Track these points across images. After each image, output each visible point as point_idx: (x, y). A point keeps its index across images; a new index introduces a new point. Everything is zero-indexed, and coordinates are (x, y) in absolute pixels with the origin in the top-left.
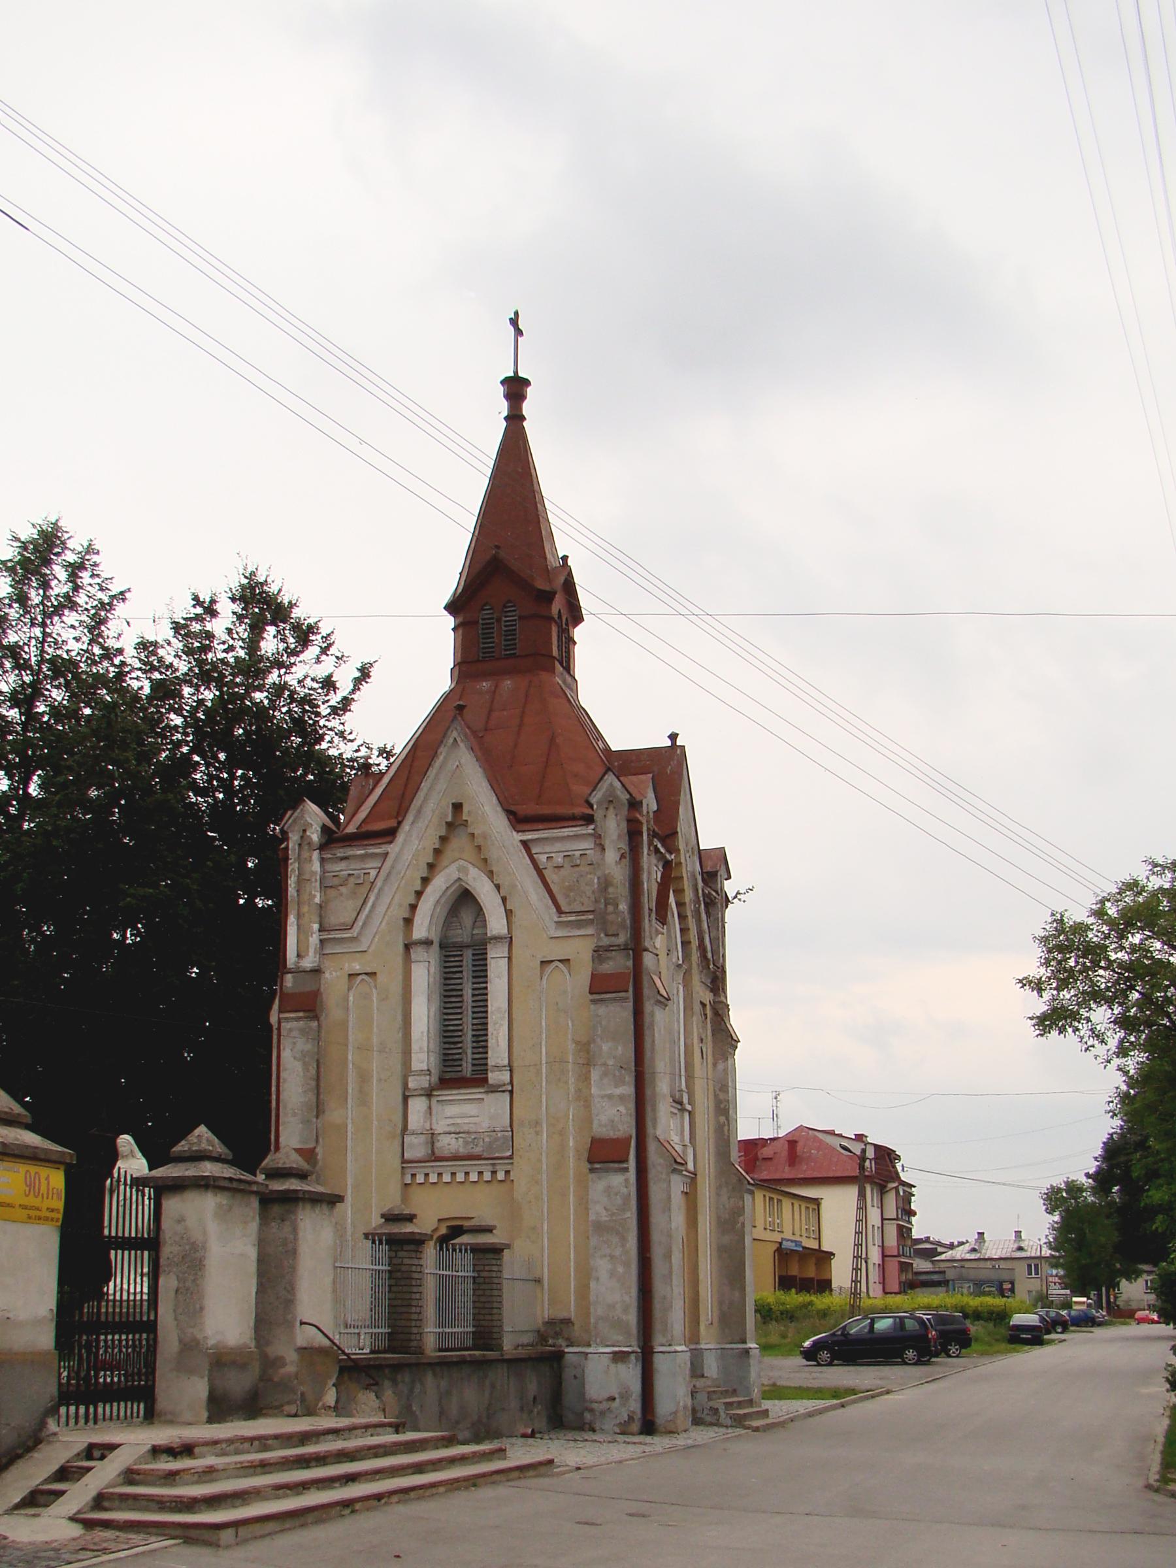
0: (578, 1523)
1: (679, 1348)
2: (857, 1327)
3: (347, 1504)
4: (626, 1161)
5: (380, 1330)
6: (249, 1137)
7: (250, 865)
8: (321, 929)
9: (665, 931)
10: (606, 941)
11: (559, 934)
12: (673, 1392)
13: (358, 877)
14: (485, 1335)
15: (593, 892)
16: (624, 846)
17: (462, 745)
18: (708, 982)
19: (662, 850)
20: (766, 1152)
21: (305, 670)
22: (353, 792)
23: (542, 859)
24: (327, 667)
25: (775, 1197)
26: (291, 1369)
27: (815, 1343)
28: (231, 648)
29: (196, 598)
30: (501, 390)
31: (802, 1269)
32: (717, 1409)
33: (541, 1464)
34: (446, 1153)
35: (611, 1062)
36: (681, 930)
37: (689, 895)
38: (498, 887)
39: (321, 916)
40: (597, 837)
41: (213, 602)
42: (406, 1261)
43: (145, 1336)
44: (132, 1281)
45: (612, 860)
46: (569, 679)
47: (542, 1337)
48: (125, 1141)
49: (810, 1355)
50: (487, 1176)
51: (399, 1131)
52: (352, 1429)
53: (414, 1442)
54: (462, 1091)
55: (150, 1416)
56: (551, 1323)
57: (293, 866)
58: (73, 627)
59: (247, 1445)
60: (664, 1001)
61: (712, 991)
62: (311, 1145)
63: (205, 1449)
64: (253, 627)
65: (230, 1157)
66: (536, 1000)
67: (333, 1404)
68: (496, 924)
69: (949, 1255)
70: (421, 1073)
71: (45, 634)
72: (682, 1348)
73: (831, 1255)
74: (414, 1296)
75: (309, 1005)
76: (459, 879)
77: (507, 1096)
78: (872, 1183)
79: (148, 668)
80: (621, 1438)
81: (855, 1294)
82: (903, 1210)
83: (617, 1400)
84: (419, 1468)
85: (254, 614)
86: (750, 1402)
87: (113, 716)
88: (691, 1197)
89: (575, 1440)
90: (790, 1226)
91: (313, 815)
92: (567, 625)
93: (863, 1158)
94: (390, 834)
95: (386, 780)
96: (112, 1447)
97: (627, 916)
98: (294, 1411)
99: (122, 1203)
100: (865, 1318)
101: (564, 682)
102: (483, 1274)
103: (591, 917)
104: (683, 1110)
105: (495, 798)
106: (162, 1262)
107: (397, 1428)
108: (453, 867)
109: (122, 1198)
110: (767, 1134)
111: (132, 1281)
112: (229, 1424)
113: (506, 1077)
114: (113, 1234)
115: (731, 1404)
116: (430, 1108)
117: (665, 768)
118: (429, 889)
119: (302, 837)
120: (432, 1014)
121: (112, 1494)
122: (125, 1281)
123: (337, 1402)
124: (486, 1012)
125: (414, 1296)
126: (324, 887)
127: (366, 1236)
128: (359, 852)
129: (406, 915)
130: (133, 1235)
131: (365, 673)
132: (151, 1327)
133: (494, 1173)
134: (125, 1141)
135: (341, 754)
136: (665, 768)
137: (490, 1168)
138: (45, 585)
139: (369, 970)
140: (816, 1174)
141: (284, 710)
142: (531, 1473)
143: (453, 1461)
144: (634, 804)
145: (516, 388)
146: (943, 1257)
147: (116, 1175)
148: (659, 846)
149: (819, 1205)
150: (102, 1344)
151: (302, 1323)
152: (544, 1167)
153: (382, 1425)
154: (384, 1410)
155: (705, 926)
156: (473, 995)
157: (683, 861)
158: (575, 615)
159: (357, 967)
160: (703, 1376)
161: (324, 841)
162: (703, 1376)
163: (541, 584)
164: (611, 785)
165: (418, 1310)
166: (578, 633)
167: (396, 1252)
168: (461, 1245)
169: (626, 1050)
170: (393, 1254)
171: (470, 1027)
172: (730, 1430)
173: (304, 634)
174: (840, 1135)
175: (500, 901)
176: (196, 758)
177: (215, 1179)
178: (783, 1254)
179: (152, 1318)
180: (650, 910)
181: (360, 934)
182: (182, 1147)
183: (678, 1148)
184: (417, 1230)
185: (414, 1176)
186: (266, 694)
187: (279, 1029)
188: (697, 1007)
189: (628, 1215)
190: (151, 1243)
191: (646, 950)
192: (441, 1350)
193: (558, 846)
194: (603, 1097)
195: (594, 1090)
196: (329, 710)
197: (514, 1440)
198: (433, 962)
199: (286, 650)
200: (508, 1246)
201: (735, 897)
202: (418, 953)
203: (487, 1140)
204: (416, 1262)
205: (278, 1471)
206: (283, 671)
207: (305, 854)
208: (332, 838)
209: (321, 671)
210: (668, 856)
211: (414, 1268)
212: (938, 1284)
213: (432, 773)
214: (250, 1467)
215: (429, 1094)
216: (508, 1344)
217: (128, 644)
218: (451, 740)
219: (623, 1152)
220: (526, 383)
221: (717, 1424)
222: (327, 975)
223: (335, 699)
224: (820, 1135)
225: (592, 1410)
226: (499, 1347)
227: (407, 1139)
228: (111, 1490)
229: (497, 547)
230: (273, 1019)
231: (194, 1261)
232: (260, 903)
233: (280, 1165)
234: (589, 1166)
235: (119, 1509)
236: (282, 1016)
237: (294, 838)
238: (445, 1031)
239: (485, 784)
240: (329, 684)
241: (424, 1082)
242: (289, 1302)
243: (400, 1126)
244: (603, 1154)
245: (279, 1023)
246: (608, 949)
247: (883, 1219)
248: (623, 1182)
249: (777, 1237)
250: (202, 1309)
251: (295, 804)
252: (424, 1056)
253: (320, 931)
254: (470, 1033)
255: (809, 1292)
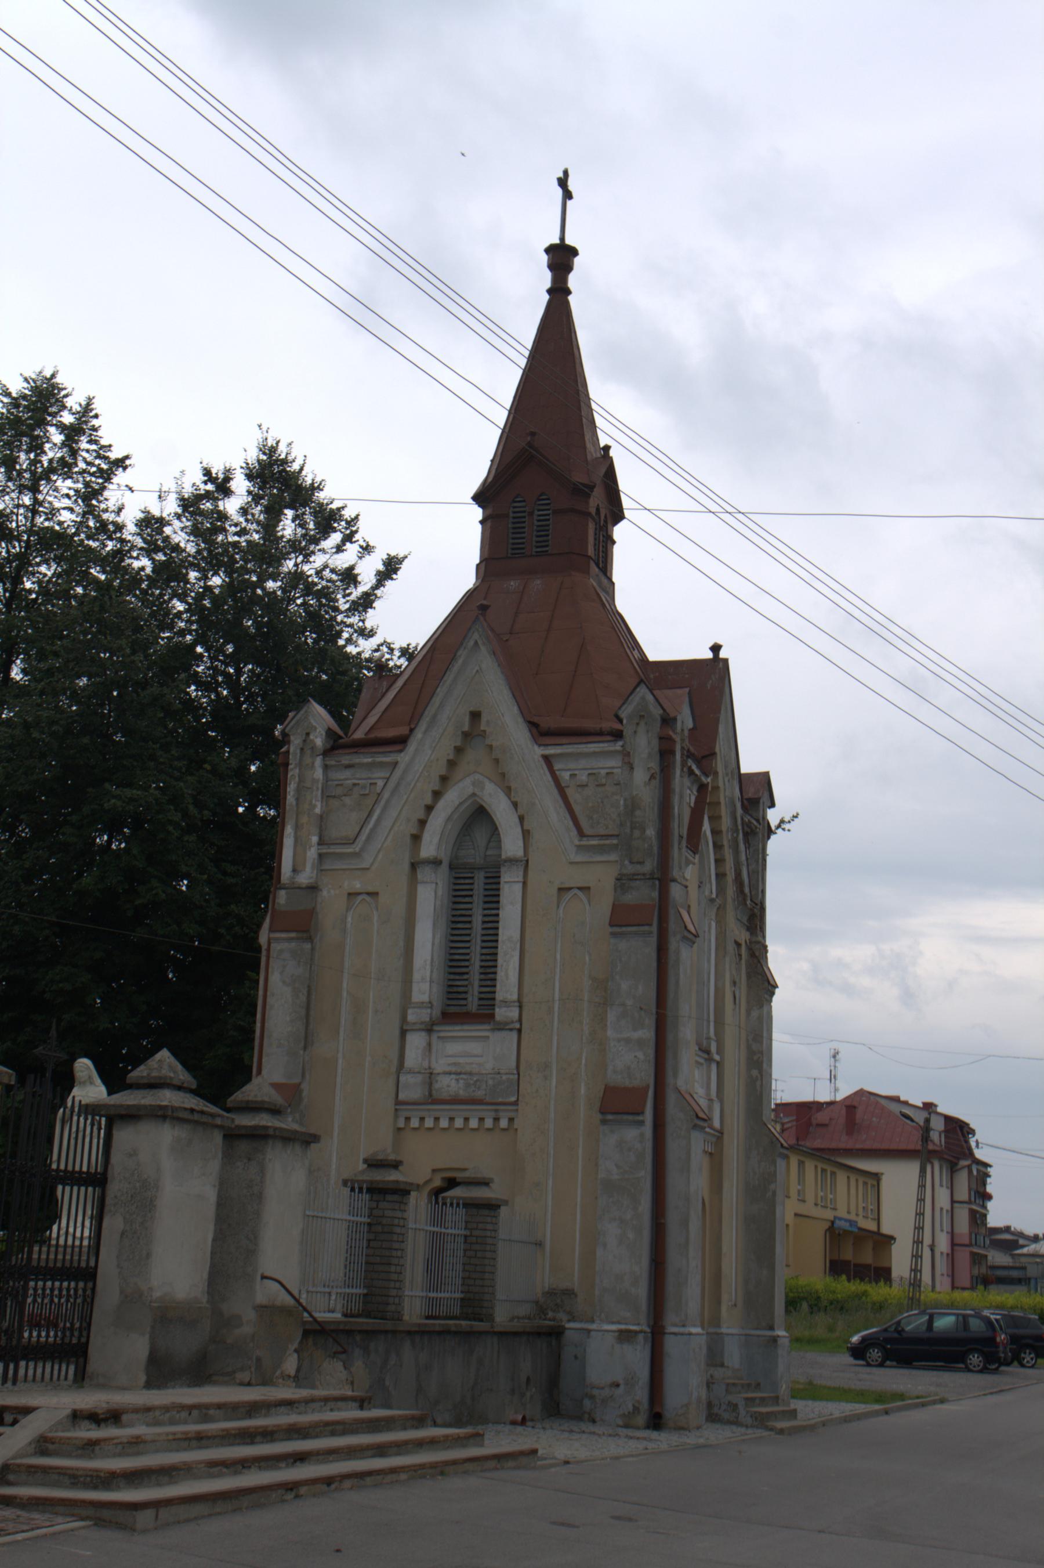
0: (554, 1523)
1: (694, 1330)
2: (914, 1323)
3: (291, 1487)
4: (642, 1113)
5: (354, 1291)
6: (222, 1065)
7: (253, 768)
8: (321, 843)
9: (696, 861)
10: (630, 869)
11: (579, 858)
12: (686, 1383)
13: (364, 787)
14: (475, 1304)
15: (619, 815)
16: (655, 765)
17: (483, 648)
18: (745, 919)
19: (697, 772)
20: (821, 1117)
21: (327, 557)
22: (365, 695)
23: (565, 776)
24: (348, 557)
25: (829, 1169)
26: (247, 1330)
27: (864, 1339)
28: (243, 532)
29: (207, 472)
30: (544, 258)
31: (858, 1253)
32: (736, 1405)
33: (522, 1453)
34: (444, 1095)
35: (629, 1002)
36: (716, 861)
37: (726, 823)
38: (515, 805)
39: (321, 828)
40: (626, 755)
41: (227, 479)
42: (388, 1213)
43: (81, 1284)
44: (79, 1224)
45: (641, 780)
46: (605, 581)
47: (541, 1310)
48: (84, 1066)
49: (858, 1352)
50: (489, 1123)
51: (394, 1069)
52: (309, 1401)
53: (378, 1420)
54: (466, 1027)
55: (81, 1378)
56: (551, 1293)
57: (293, 772)
58: (68, 496)
59: (184, 1414)
60: (691, 938)
61: (748, 929)
62: (296, 1081)
63: (135, 1416)
64: (267, 510)
65: (194, 1086)
66: (552, 928)
67: (293, 1373)
68: (512, 845)
69: (1032, 1248)
70: (421, 1005)
71: (36, 502)
72: (698, 1330)
73: (891, 1239)
74: (394, 1253)
75: (303, 925)
76: (474, 794)
77: (514, 1035)
78: (941, 1159)
79: (151, 549)
80: (620, 1431)
81: (916, 1283)
82: (977, 1192)
83: (622, 1387)
84: (381, 1450)
85: (272, 495)
86: (776, 1400)
87: (106, 598)
88: (716, 1158)
89: (571, 1431)
90: (845, 1202)
91: (318, 717)
92: (606, 521)
93: (927, 1129)
94: (401, 741)
95: (400, 682)
96: (27, 1411)
97: (655, 843)
98: (247, 1380)
99: (73, 1135)
100: (923, 1312)
101: (600, 583)
102: (475, 1233)
103: (615, 842)
104: (710, 1060)
105: (516, 708)
106: (109, 1200)
107: (362, 1403)
108: (468, 781)
109: (74, 1129)
110: (824, 1097)
111: (79, 1224)
112: (170, 1391)
113: (514, 1013)
114: (62, 1167)
115: (752, 1399)
116: (429, 1044)
117: (706, 681)
118: (441, 804)
119: (304, 741)
120: (437, 941)
121: (19, 1465)
122: (72, 1224)
123: (298, 1370)
124: (497, 941)
125: (394, 1253)
126: (327, 797)
127: (345, 1183)
128: (366, 760)
129: (414, 832)
130: (85, 1169)
131: (391, 567)
132: (90, 1275)
133: (496, 1120)
134: (84, 1066)
135: (359, 654)
136: (706, 681)
137: (493, 1114)
138: (37, 447)
139: (371, 889)
140: (885, 1146)
141: (299, 602)
142: (511, 1464)
143: (420, 1444)
144: (668, 721)
145: (561, 258)
146: (1025, 1250)
147: (69, 1104)
148: (694, 767)
149: (879, 1181)
150: (31, 1292)
151: (264, 1277)
152: (552, 1115)
153: (344, 1399)
154: (352, 1383)
155: (743, 857)
156: (484, 922)
157: (721, 784)
158: (615, 511)
159: (357, 886)
160: (722, 1365)
161: (328, 746)
162: (722, 1365)
163: (579, 477)
164: (643, 698)
165: (398, 1269)
166: (620, 532)
167: (378, 1201)
168: (452, 1198)
169: (646, 990)
170: (374, 1205)
171: (478, 957)
172: (750, 1431)
173: (327, 519)
174: (906, 1103)
175: (517, 820)
176: (199, 649)
177: (174, 1109)
178: (835, 1234)
179: (92, 1263)
180: (681, 837)
181: (362, 849)
182: (140, 1073)
183: (703, 1102)
184: (401, 1178)
185: (408, 1119)
186: (279, 584)
187: (268, 950)
188: (731, 947)
189: (642, 1173)
190: (98, 1180)
191: (674, 880)
192: (428, 1317)
193: (583, 763)
194: (619, 1040)
195: (609, 1033)
196: (347, 606)
197: (500, 1427)
198: (440, 885)
199: (304, 536)
200: (506, 1203)
201: (779, 826)
202: (425, 873)
203: (490, 1082)
204: (399, 1214)
205: (217, 1446)
206: (300, 559)
207: (308, 760)
208: (336, 744)
209: (342, 561)
210: (703, 779)
211: (396, 1221)
212: (1019, 1281)
213: (449, 677)
214: (186, 1439)
215: (429, 1029)
216: (502, 1317)
217: (130, 518)
218: (472, 643)
219: (643, 1104)
220: (573, 252)
221: (736, 1423)
222: (325, 893)
223: (356, 593)
224: (883, 1102)
225: (592, 1397)
226: (491, 1318)
227: (403, 1078)
228: (18, 1461)
229: (533, 434)
230: (263, 939)
231: (144, 1201)
232: (261, 812)
233: (250, 1098)
234: (599, 1116)
235: (25, 1484)
236: (272, 935)
237: (296, 741)
238: (452, 960)
239: (506, 693)
240: (349, 576)
241: (425, 1015)
242: (251, 1253)
243: (395, 1062)
244: (616, 1104)
245: (269, 943)
246: (632, 877)
247: (953, 1202)
248: (637, 1136)
249: (829, 1215)
250: (148, 1255)
251: (301, 701)
252: (426, 987)
253: (319, 844)
254: (478, 964)
255: (862, 1280)
